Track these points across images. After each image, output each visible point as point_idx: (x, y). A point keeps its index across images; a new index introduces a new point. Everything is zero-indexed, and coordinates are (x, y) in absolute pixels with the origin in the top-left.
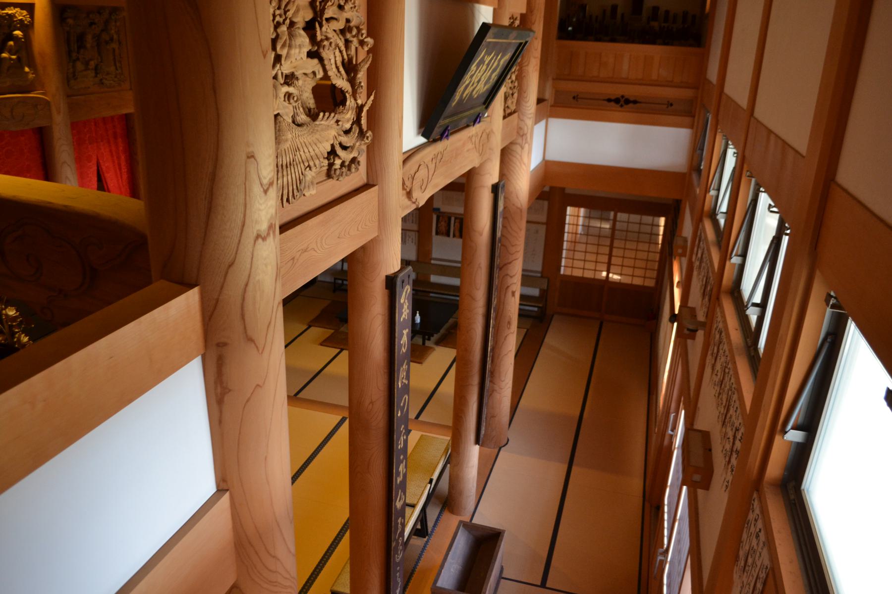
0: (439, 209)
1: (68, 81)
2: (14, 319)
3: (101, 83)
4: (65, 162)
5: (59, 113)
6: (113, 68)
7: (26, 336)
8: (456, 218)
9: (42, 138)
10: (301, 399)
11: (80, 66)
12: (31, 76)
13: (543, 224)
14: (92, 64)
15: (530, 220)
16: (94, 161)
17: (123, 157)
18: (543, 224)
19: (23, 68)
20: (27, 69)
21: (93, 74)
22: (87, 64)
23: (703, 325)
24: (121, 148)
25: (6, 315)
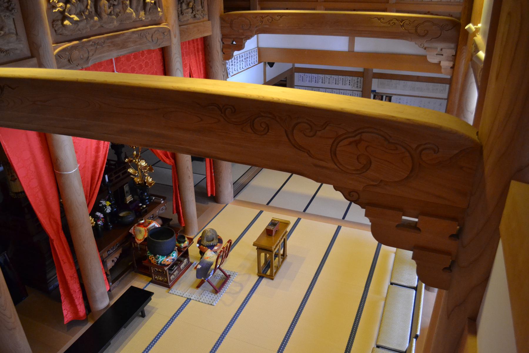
0: (375, 91)
1: (179, 16)
2: (145, 168)
3: (195, 16)
4: (178, 69)
5: (175, 37)
6: (200, 7)
7: (150, 178)
8: (386, 97)
9: (164, 54)
10: (271, 207)
11: (184, 6)
12: (161, 14)
13: (445, 99)
14: (191, 4)
15: (158, 65)
16: (188, 67)
17: (202, 63)
18: (445, 99)
19: (157, 9)
20: (159, 9)
21: (191, 11)
22: (188, 4)
23: (181, 270)
24: (201, 58)
25: (141, 165)
